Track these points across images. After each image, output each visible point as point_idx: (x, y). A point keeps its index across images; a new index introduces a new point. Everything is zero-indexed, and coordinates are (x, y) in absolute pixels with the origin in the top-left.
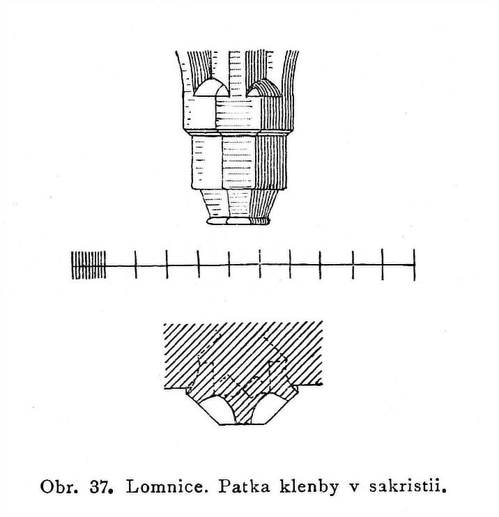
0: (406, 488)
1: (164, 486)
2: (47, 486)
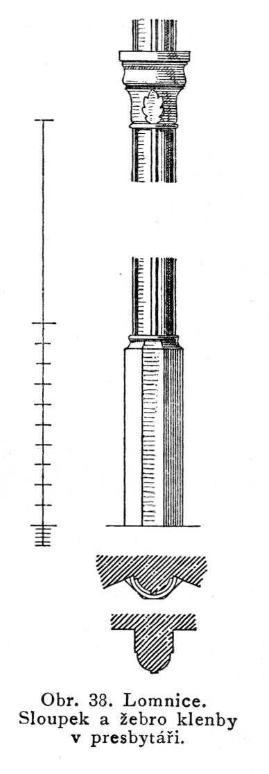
2: (48, 699)
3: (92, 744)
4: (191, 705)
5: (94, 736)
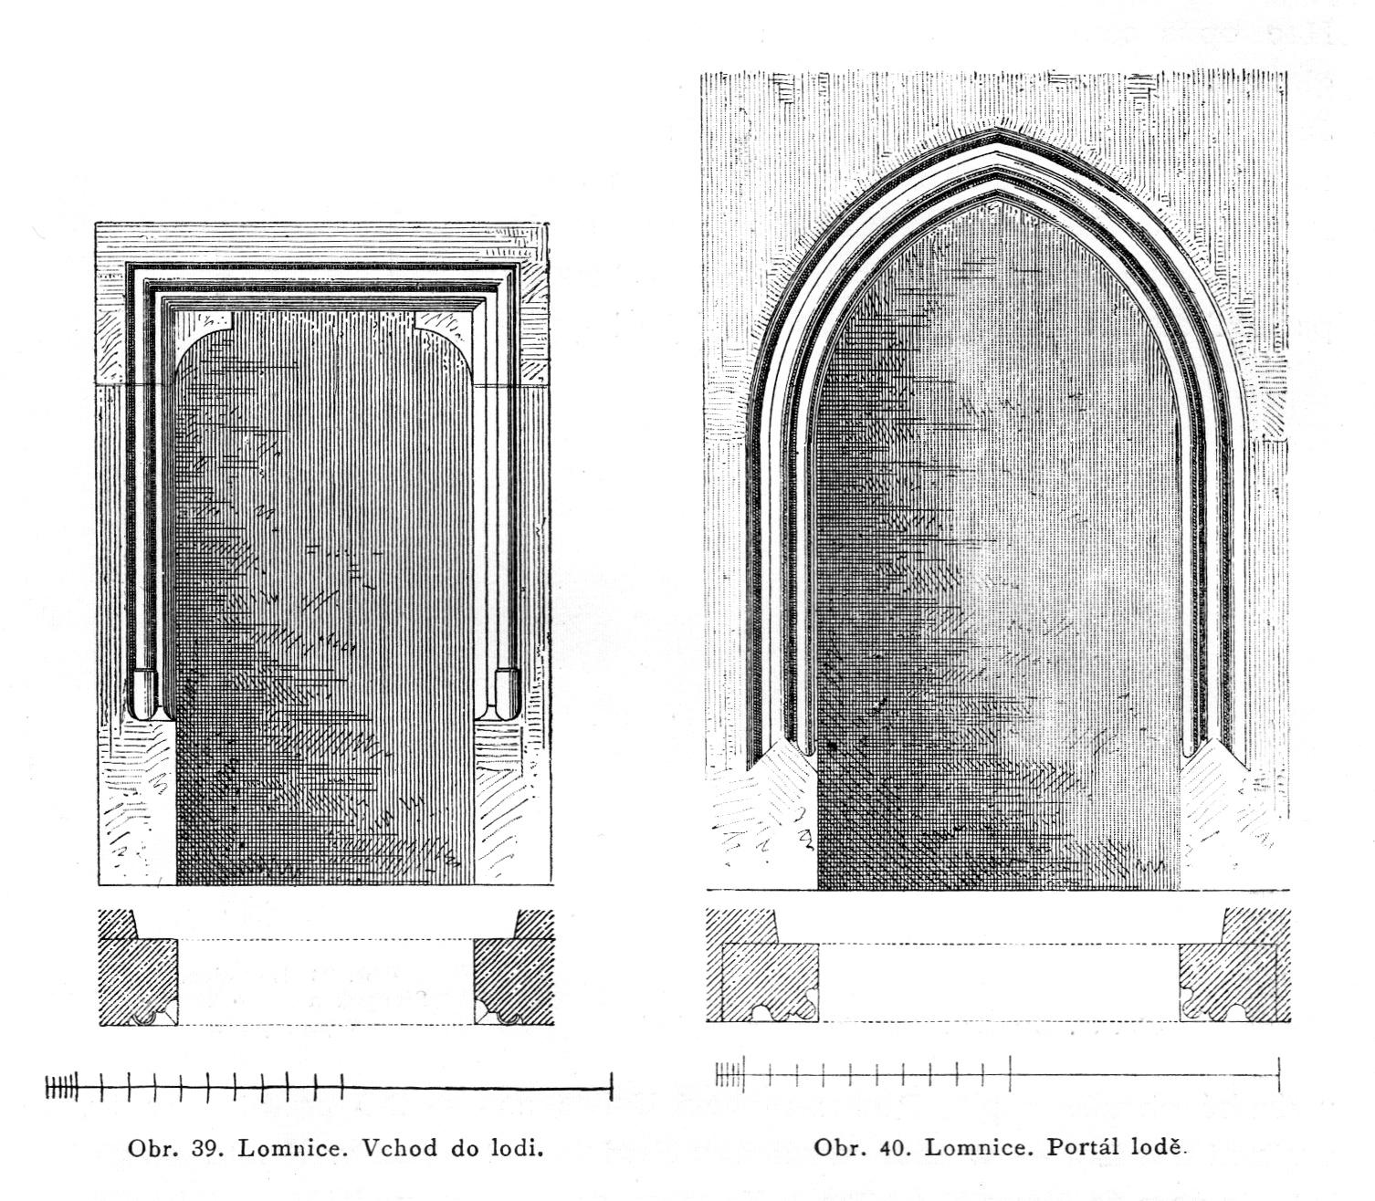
0: (1088, 1149)
1: (288, 1147)
2: (823, 1147)
3: (1049, 1151)
4: (329, 1153)
5: (434, 1154)
